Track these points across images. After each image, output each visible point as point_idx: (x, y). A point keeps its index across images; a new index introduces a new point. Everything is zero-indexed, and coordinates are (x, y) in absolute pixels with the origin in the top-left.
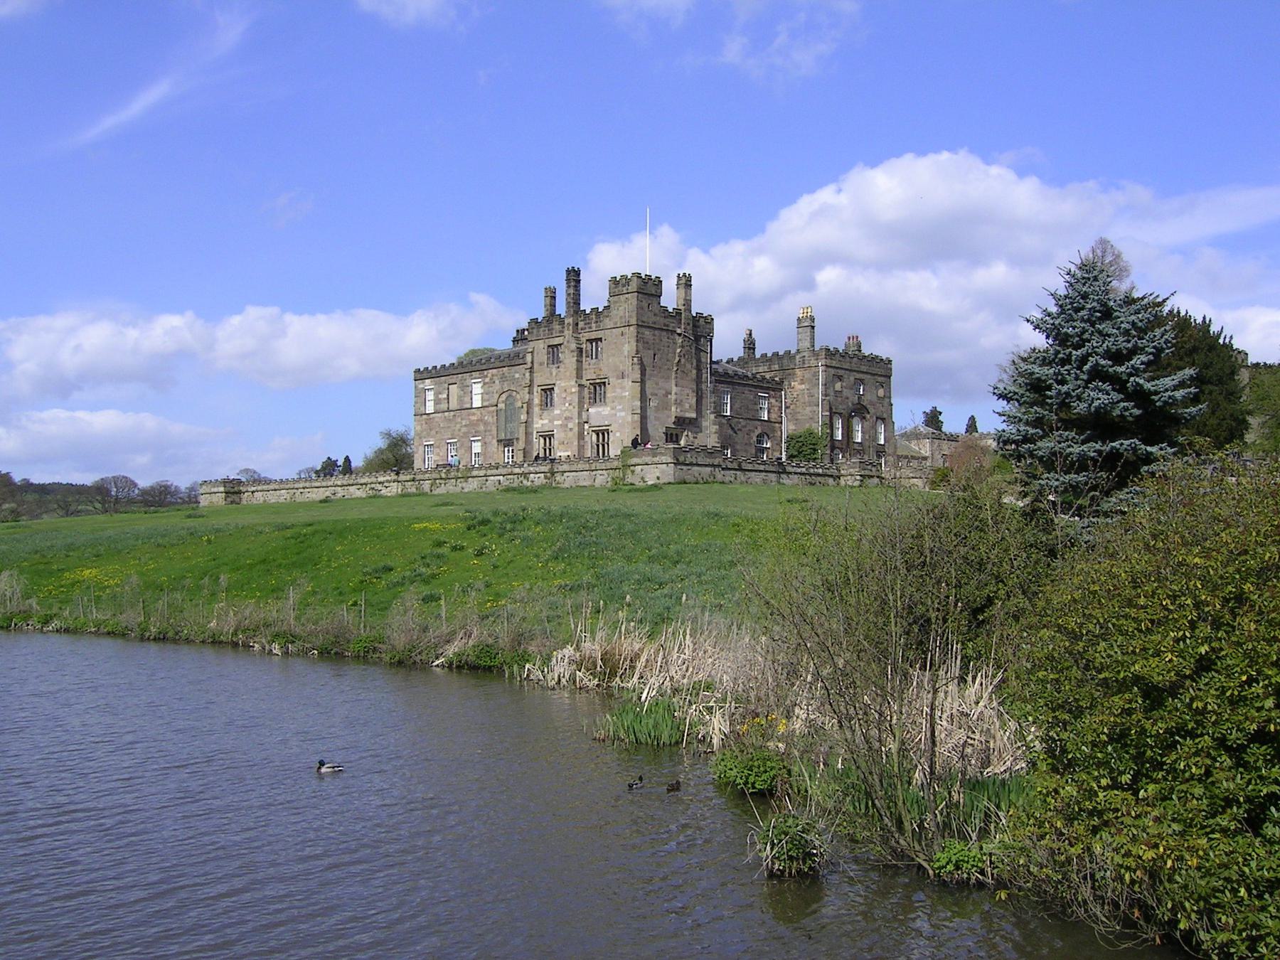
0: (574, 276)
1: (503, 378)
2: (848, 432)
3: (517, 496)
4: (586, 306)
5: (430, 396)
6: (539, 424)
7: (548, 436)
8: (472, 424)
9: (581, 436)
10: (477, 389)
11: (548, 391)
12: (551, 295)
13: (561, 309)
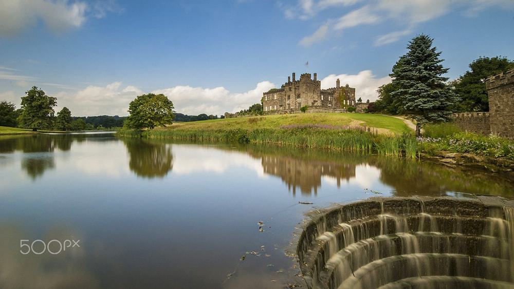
0: (294, 74)
1: (280, 94)
2: (346, 103)
3: (493, 90)
4: (296, 80)
5: (266, 97)
6: (288, 102)
7: (289, 104)
8: (275, 103)
9: (296, 104)
10: (275, 96)
11: (289, 96)
12: (289, 78)
13: (291, 81)
